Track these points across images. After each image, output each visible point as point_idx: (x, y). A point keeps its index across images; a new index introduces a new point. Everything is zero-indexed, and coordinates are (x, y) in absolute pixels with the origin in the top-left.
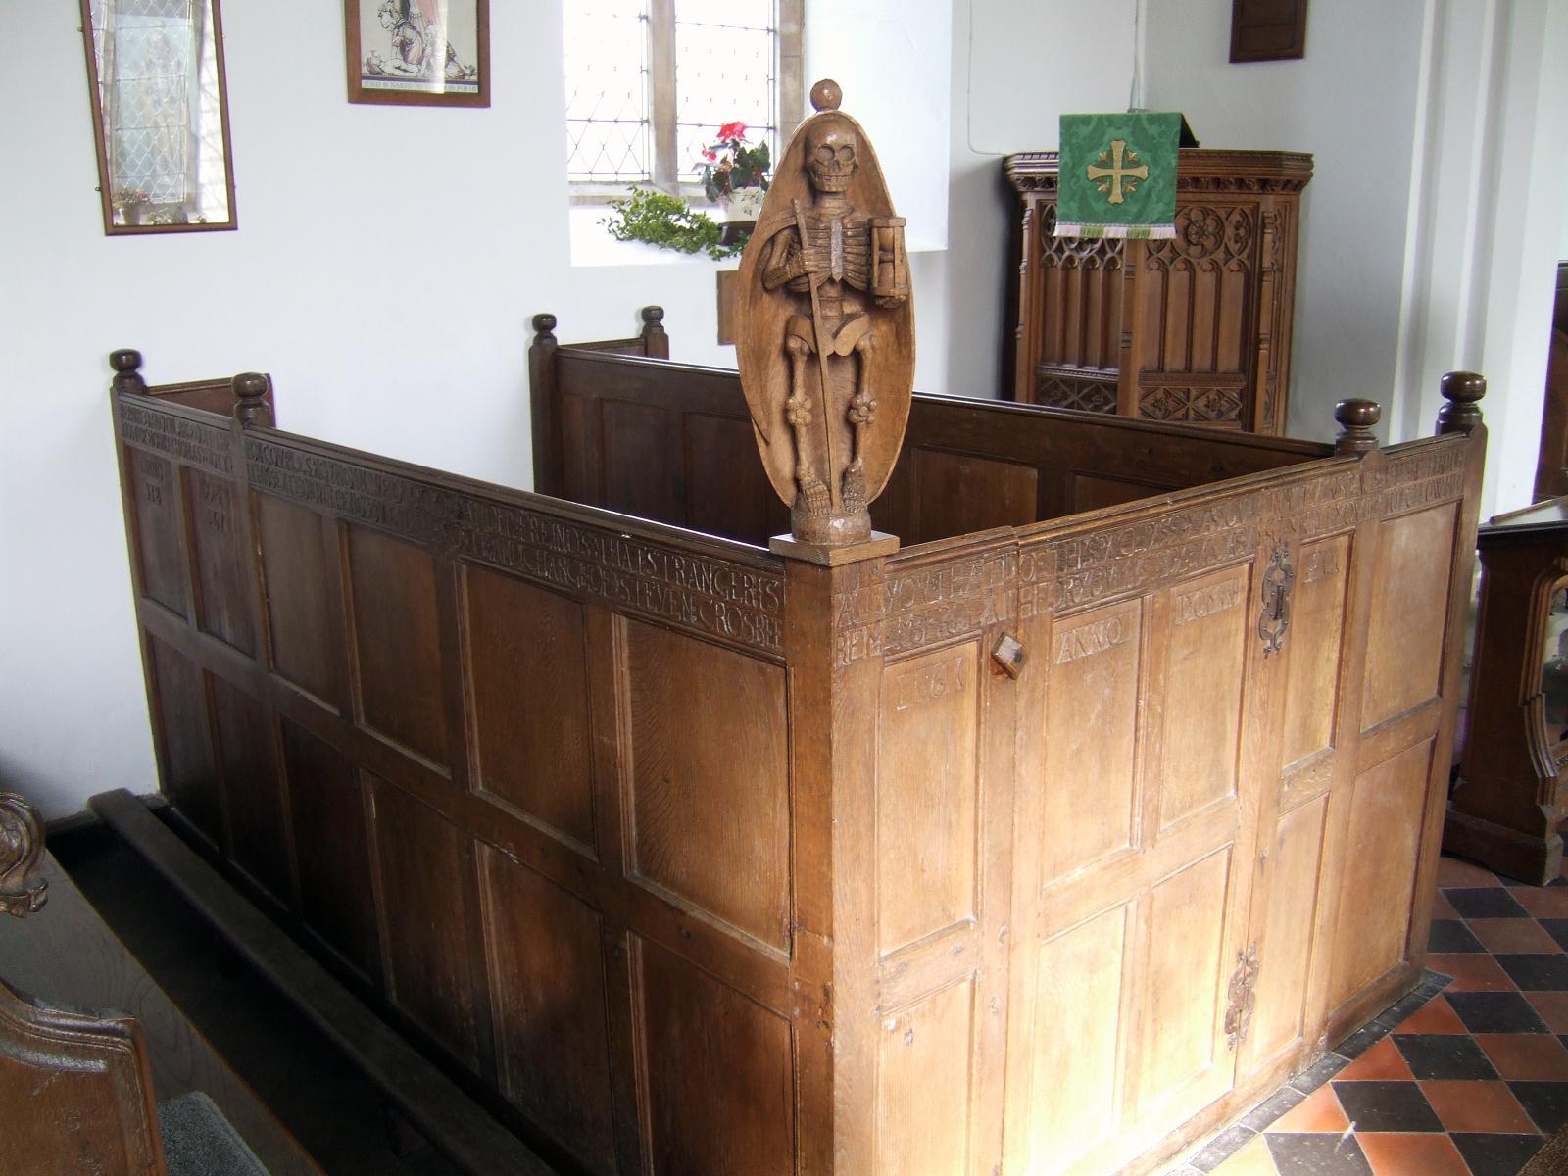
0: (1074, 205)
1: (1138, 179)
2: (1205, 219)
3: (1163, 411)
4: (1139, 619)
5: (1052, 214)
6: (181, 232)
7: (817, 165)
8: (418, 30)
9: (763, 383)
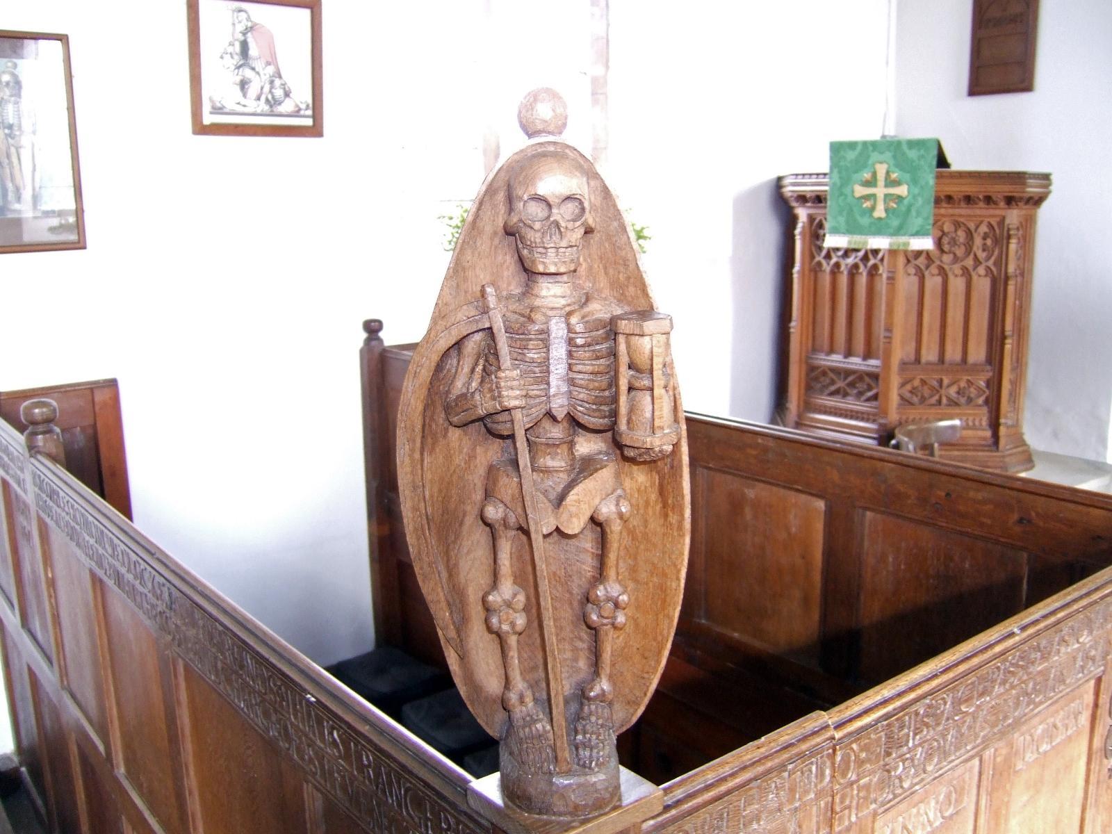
0: (842, 220)
2: (956, 231)
3: (919, 397)
4: (976, 778)
5: (821, 226)
6: (28, 252)
7: (524, 230)
8: (257, 70)
9: (452, 562)
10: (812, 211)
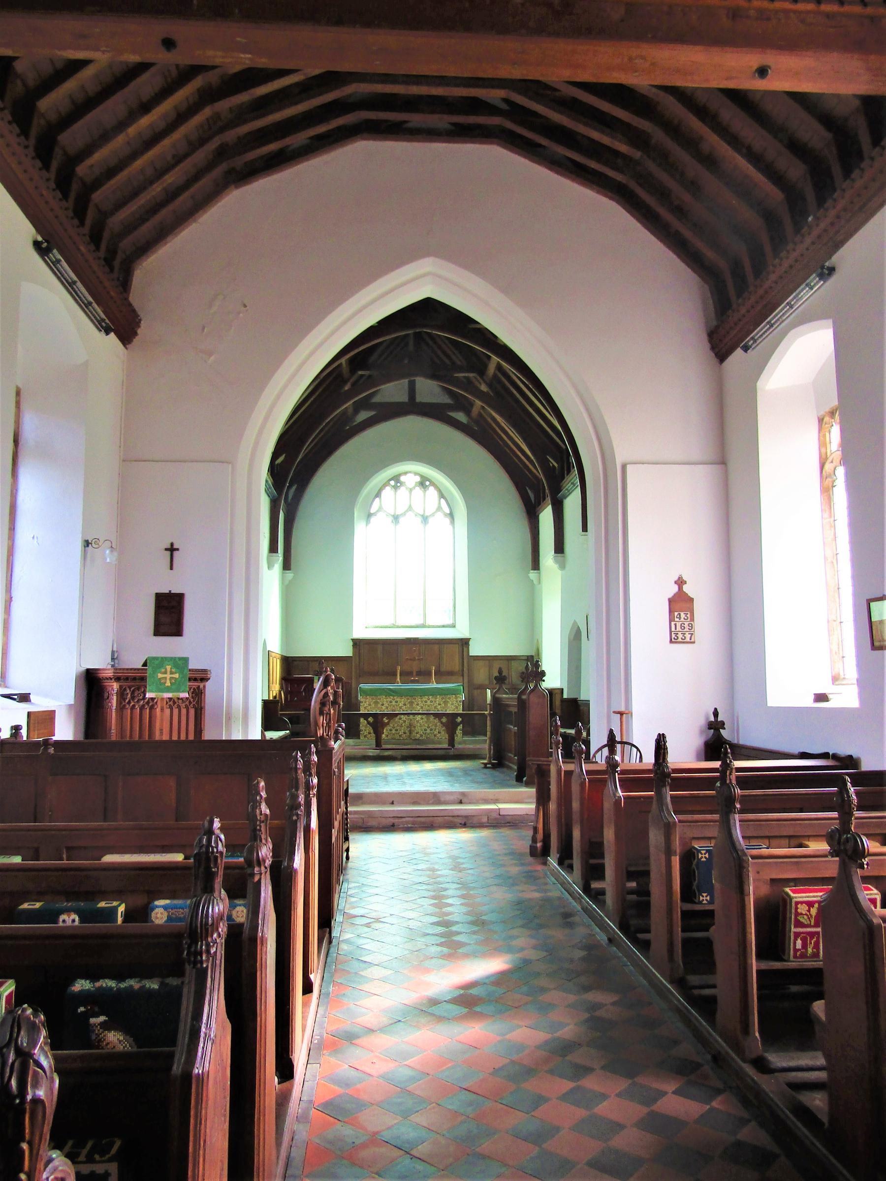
1: (175, 678)
10: (122, 684)
